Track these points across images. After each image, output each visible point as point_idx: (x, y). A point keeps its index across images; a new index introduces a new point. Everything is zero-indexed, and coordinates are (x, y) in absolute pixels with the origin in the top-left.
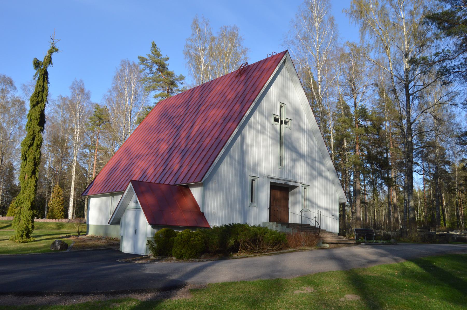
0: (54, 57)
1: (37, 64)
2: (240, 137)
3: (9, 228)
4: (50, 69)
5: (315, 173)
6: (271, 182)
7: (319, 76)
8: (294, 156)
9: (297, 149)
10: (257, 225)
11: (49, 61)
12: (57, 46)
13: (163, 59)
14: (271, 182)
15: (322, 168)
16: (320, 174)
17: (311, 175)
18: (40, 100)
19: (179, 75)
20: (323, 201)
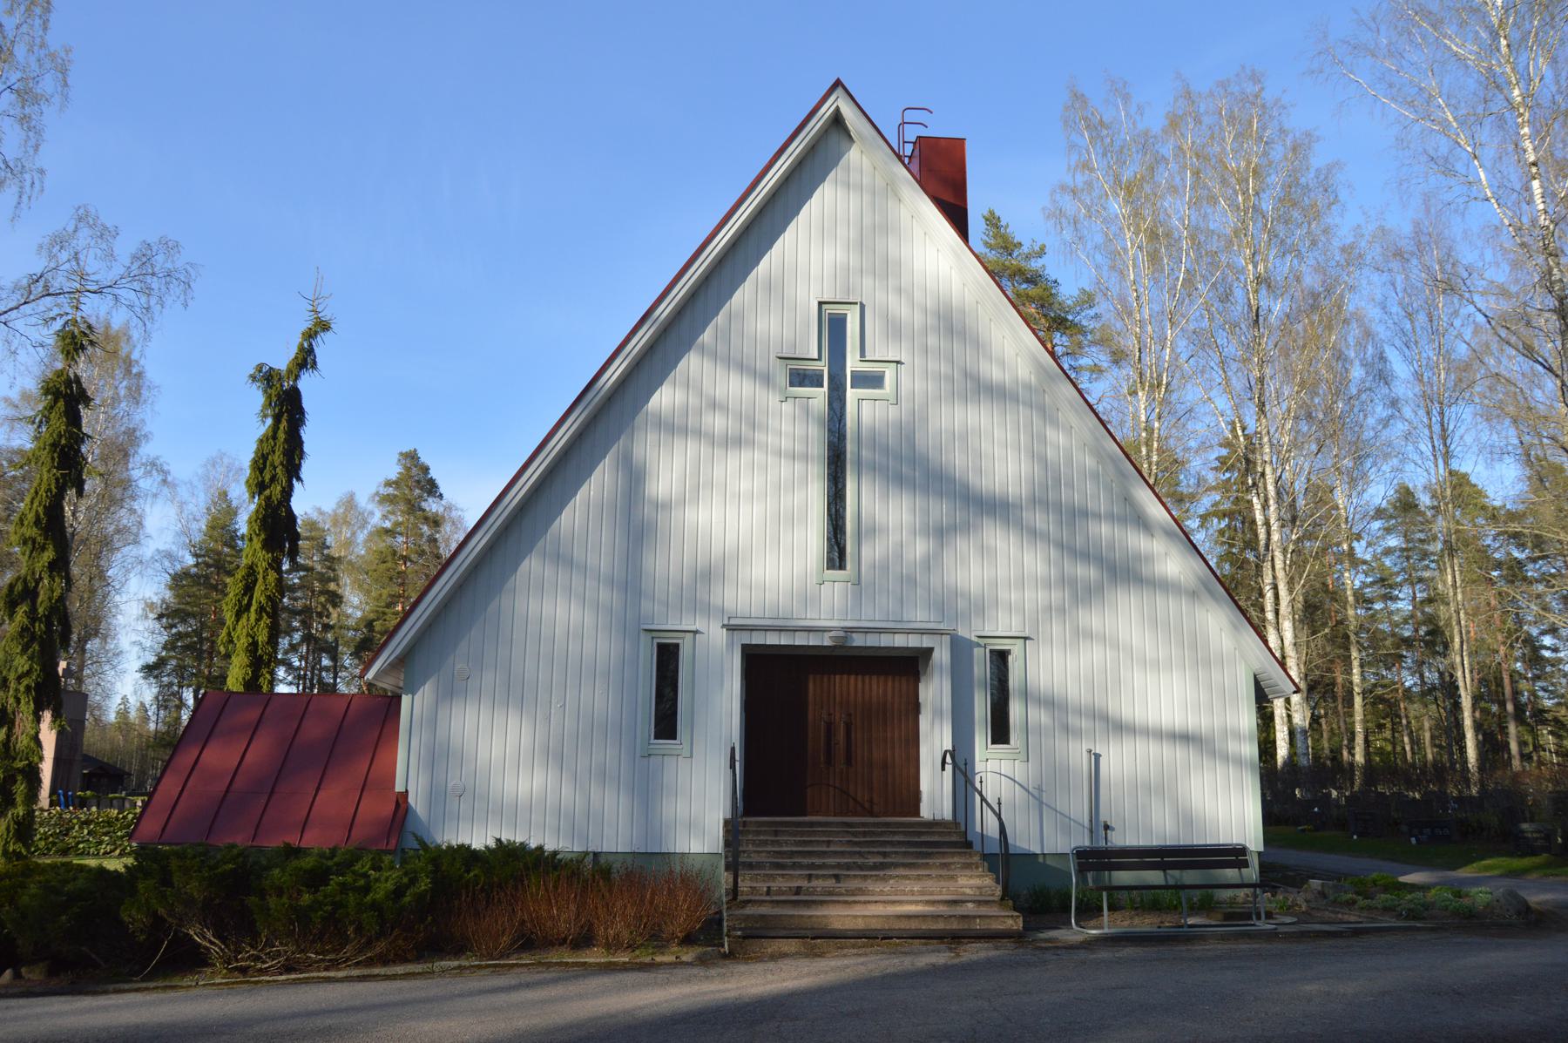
0: (324, 348)
1: (267, 377)
2: (600, 483)
3: (1102, 761)
4: (307, 384)
5: (1086, 572)
6: (745, 647)
7: (1528, 145)
8: (941, 510)
9: (966, 486)
10: (533, 845)
11: (305, 360)
12: (326, 315)
13: (1028, 257)
14: (745, 647)
15: (1137, 541)
16: (1125, 573)
17: (1065, 581)
18: (267, 478)
19: (1076, 293)
20: (1163, 696)
